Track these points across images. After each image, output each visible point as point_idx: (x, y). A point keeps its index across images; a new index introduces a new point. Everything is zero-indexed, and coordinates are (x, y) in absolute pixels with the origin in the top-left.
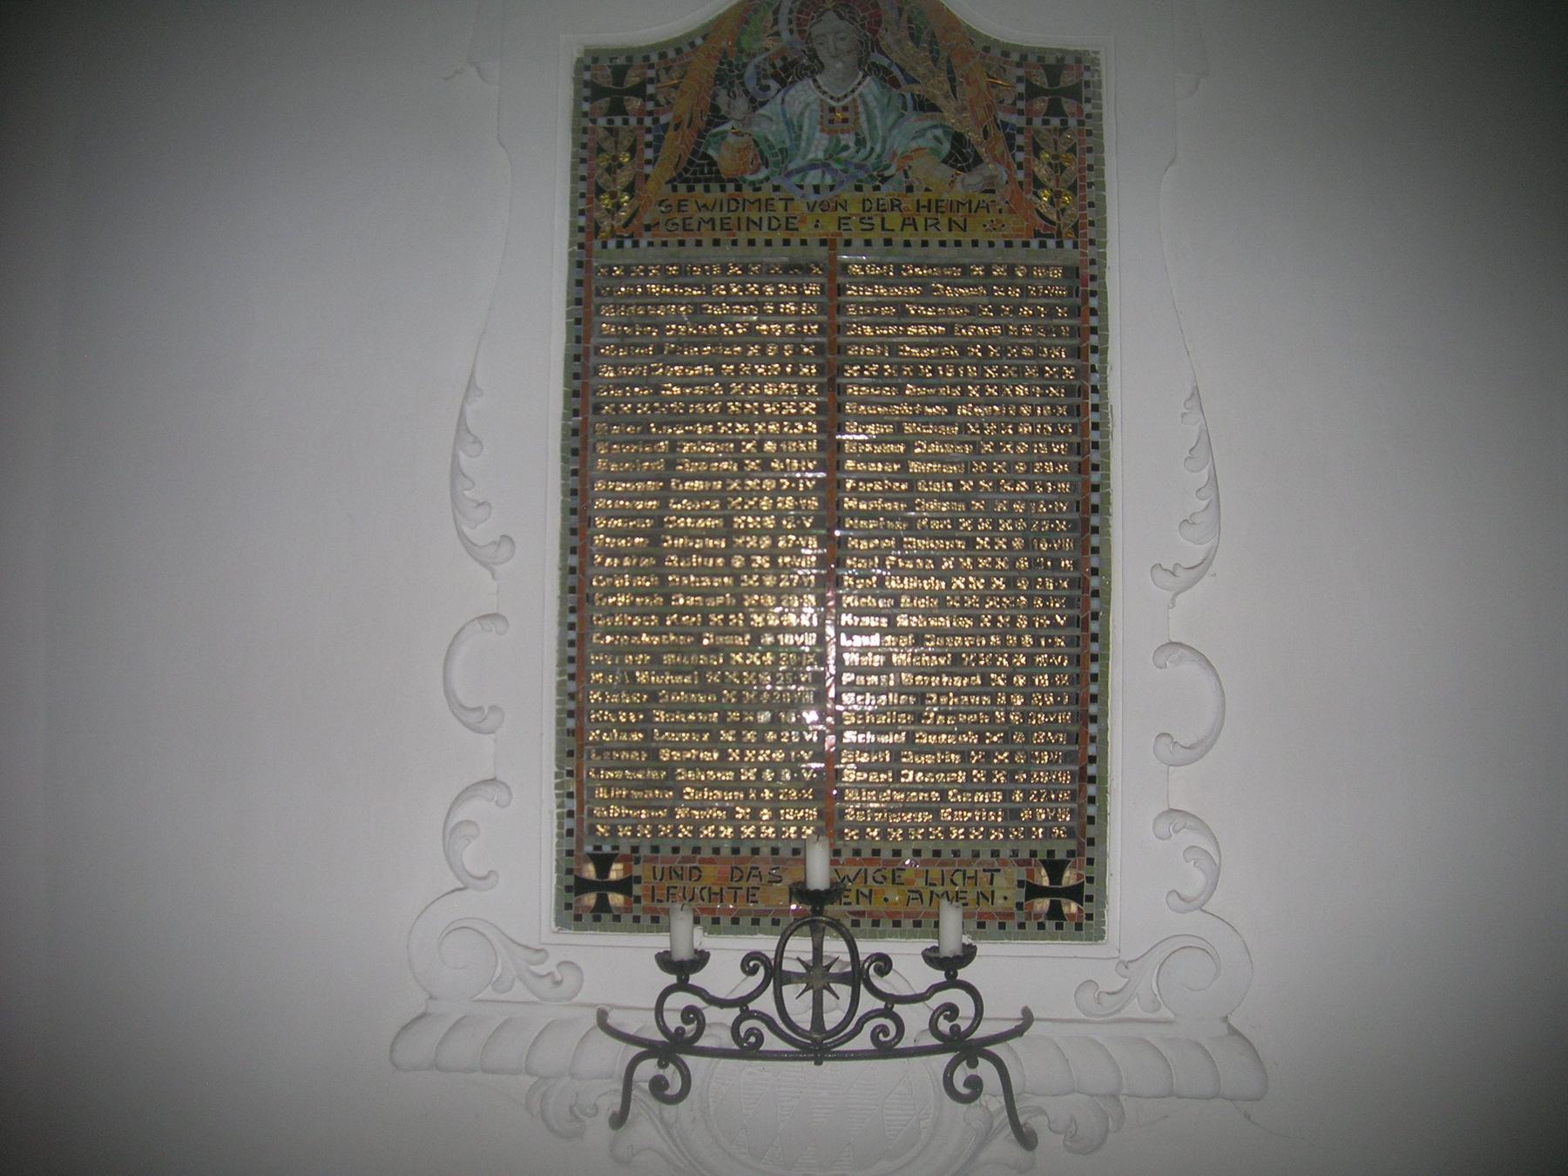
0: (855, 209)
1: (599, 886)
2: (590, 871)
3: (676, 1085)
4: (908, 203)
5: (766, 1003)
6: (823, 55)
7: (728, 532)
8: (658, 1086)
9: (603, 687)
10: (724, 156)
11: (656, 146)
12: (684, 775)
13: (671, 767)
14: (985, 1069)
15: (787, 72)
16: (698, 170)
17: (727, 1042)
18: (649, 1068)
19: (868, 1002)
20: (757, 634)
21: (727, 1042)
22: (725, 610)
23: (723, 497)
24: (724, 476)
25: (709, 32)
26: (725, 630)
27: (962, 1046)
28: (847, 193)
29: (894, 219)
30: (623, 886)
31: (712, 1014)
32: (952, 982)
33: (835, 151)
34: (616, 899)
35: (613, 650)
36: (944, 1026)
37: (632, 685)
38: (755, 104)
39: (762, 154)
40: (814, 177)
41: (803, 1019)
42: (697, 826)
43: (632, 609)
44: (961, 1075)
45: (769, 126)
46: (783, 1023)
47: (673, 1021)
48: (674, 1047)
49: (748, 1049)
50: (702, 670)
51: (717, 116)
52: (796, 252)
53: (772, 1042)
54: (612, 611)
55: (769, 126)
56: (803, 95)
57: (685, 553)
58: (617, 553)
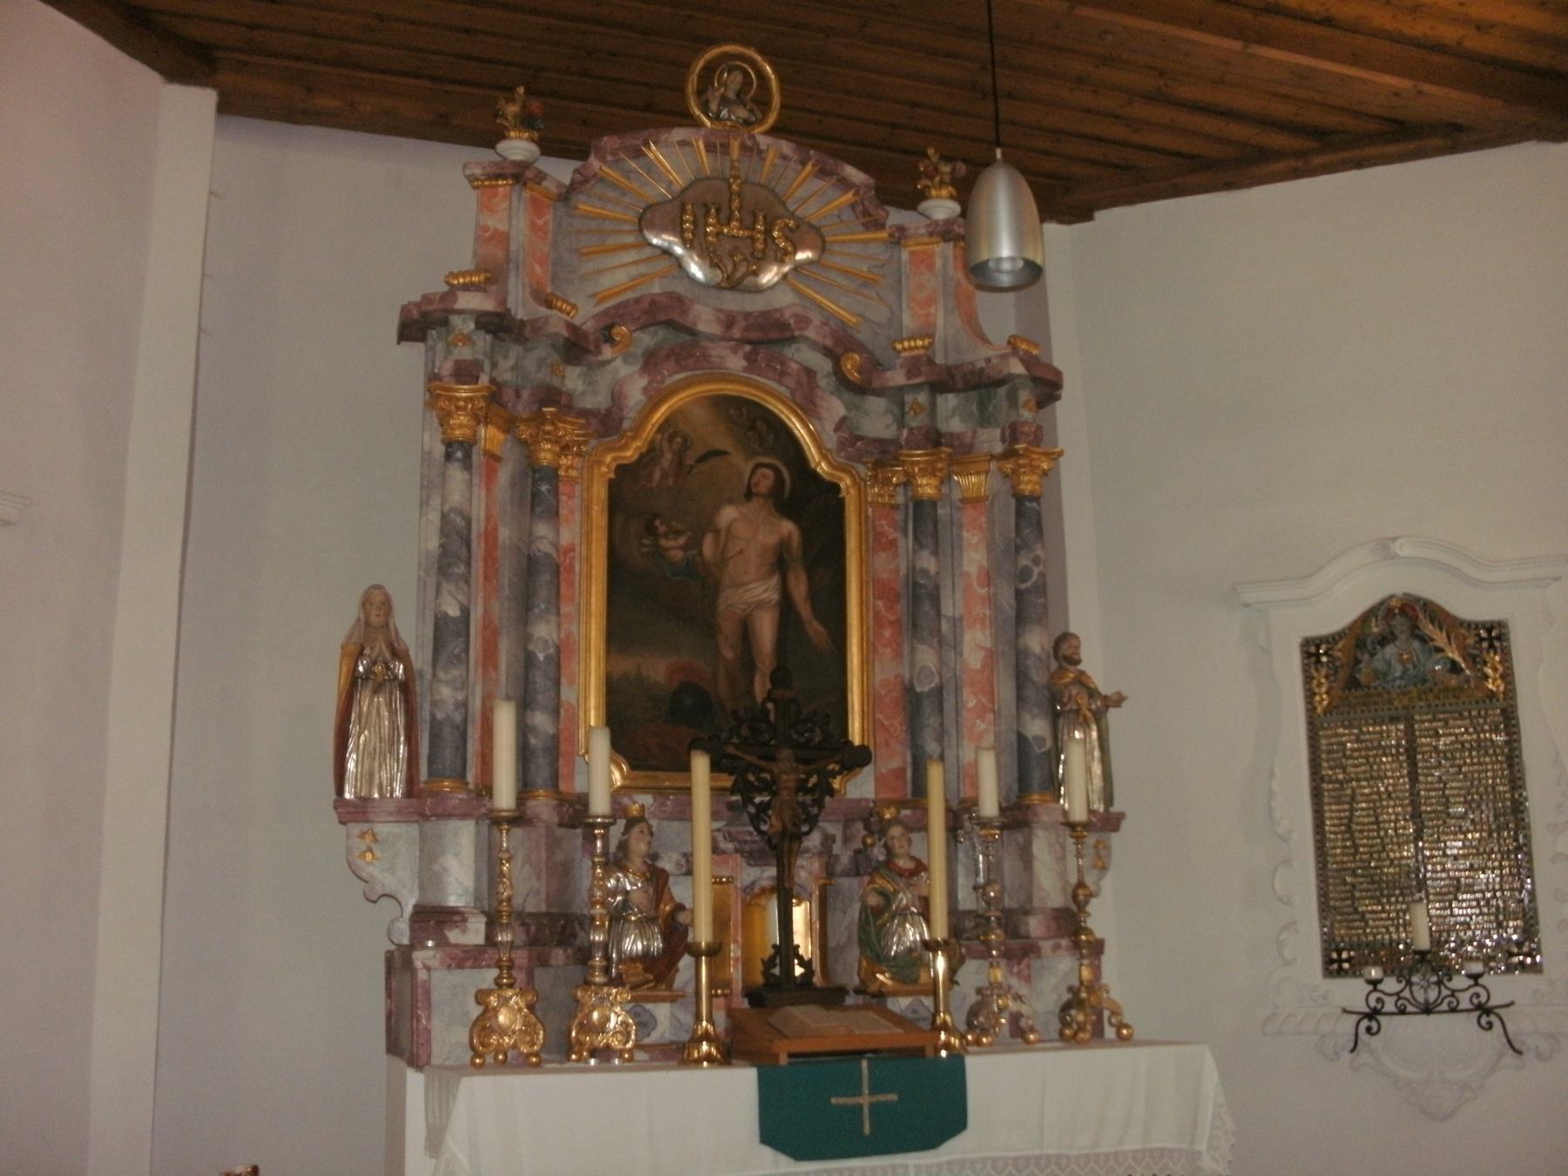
0: (1415, 694)
1: (1333, 967)
2: (1335, 955)
3: (1375, 1028)
4: (1436, 690)
5: (1406, 994)
6: (1397, 632)
7: (1377, 822)
8: (1369, 1029)
9: (1335, 885)
10: (1362, 678)
11: (1336, 674)
12: (1368, 916)
13: (1363, 914)
14: (1493, 1018)
15: (1383, 641)
16: (1353, 683)
17: (1393, 1009)
18: (1365, 1023)
19: (1445, 992)
20: (1392, 861)
21: (1393, 1009)
22: (1379, 852)
23: (1375, 809)
24: (1374, 801)
25: (1352, 627)
26: (1379, 859)
27: (1484, 1009)
28: (1411, 688)
29: (1431, 697)
30: (1349, 960)
31: (1386, 999)
32: (1476, 984)
33: (1405, 672)
34: (1346, 966)
35: (1337, 870)
36: (1475, 1001)
37: (1345, 883)
38: (1372, 655)
39: (1377, 675)
40: (1398, 683)
41: (1421, 999)
42: (1375, 935)
43: (1343, 854)
44: (1484, 1020)
45: (1378, 663)
46: (1415, 1003)
47: (1373, 1003)
48: (1373, 1014)
49: (1402, 1012)
50: (1372, 876)
51: (1358, 661)
52: (1393, 713)
53: (1410, 1008)
54: (1335, 855)
55: (1378, 663)
56: (1390, 650)
57: (1361, 831)
58: (1335, 833)
